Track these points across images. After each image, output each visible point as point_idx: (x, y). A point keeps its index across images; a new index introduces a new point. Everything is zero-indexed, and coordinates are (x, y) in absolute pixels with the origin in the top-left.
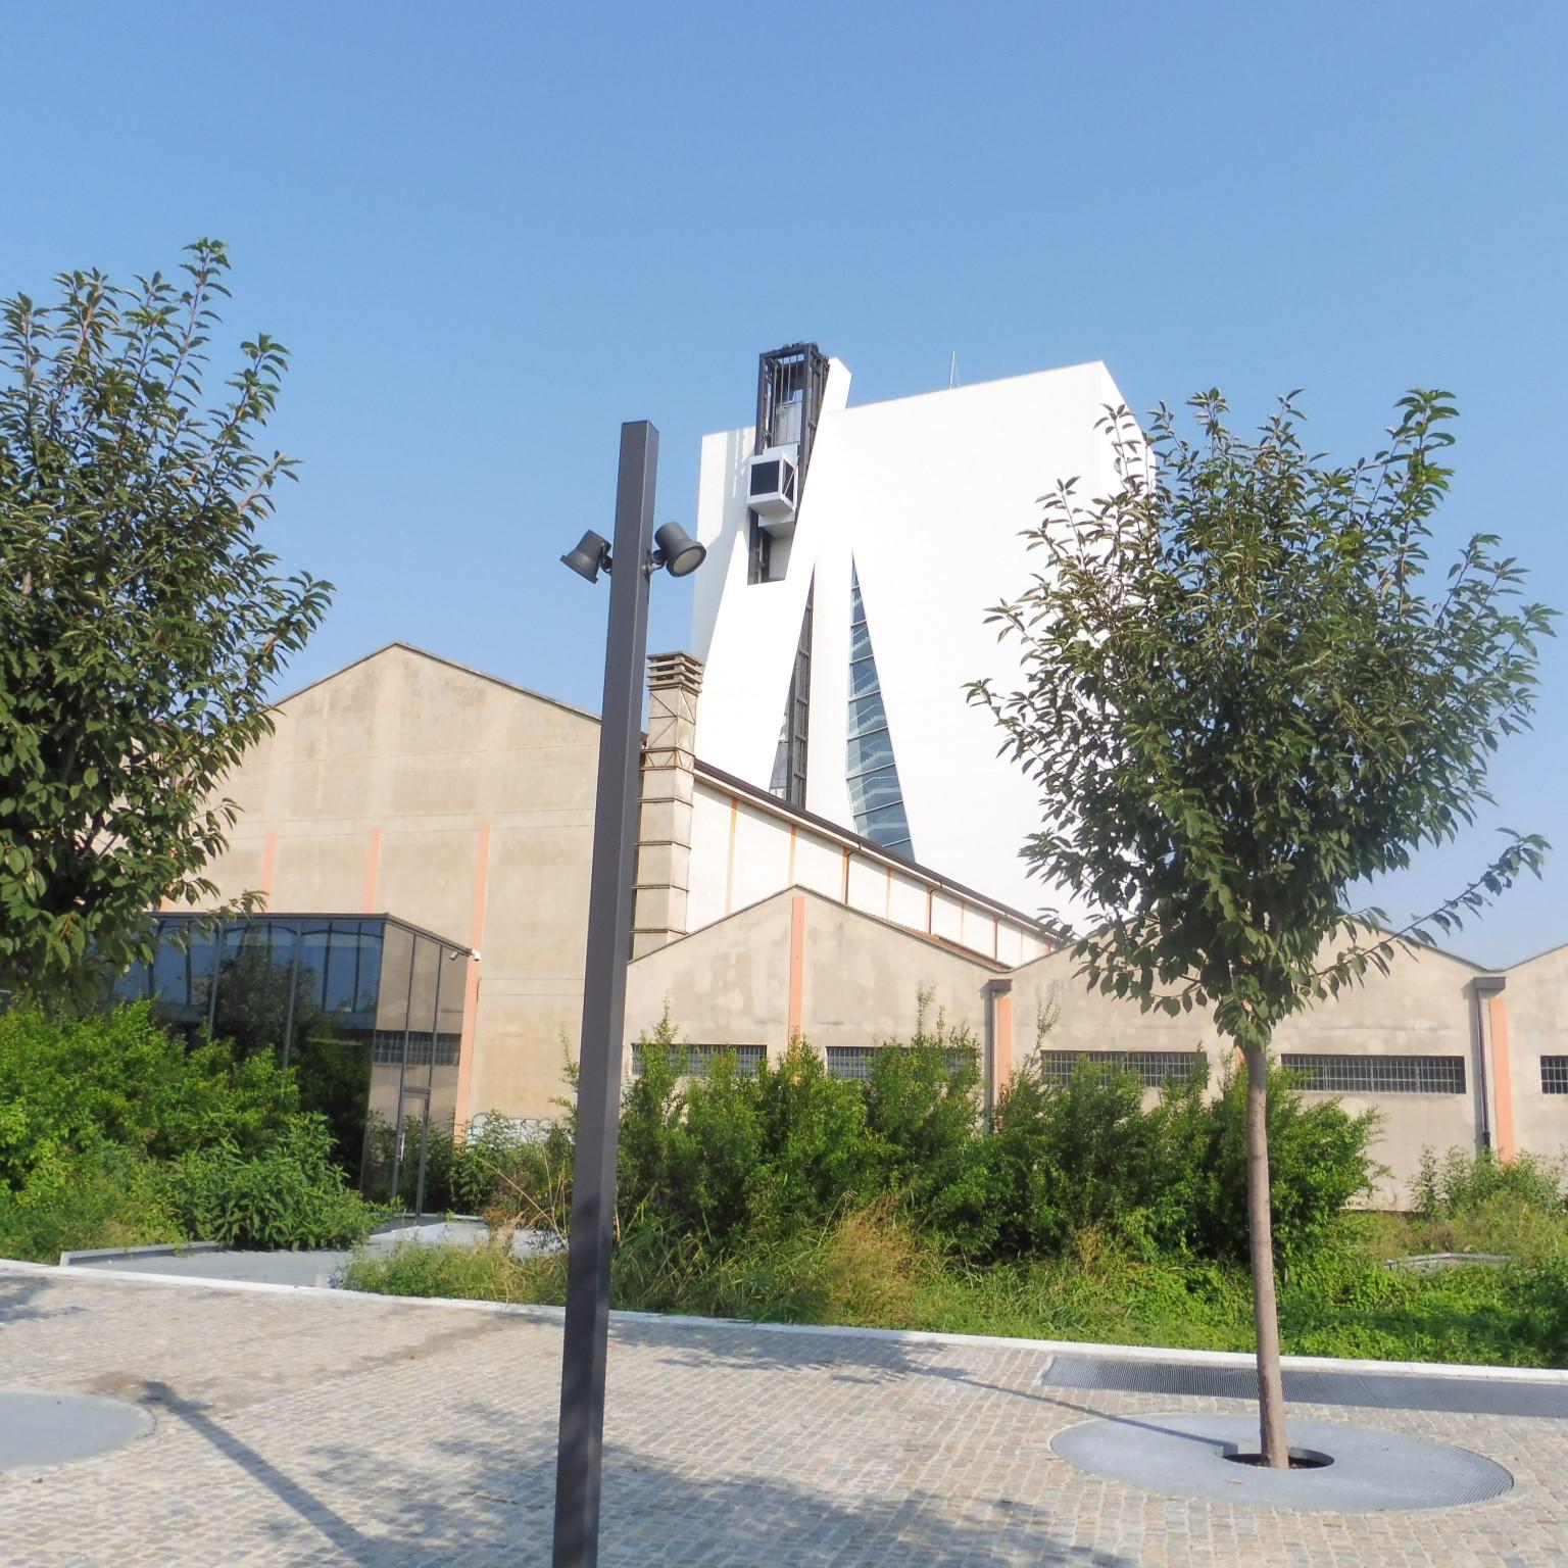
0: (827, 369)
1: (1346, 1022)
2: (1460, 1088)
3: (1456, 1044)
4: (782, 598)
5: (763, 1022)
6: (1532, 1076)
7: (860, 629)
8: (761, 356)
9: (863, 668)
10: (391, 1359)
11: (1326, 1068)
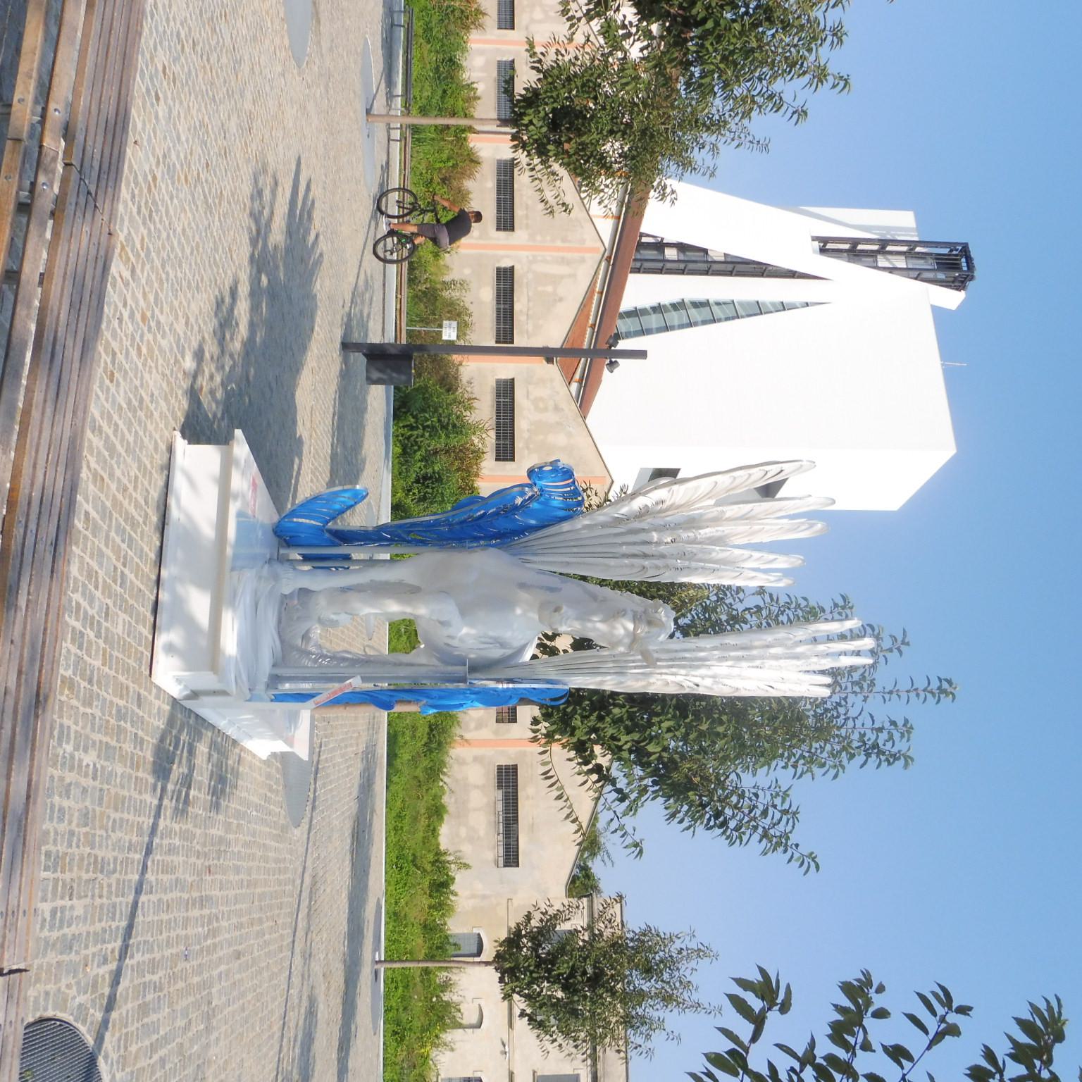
0: (958, 289)
1: (530, 294)
2: (497, 342)
3: (519, 341)
4: (808, 259)
5: (527, 28)
6: (505, 375)
7: (783, 307)
8: (967, 244)
9: (758, 309)
10: (49, 595)
11: (507, 306)
